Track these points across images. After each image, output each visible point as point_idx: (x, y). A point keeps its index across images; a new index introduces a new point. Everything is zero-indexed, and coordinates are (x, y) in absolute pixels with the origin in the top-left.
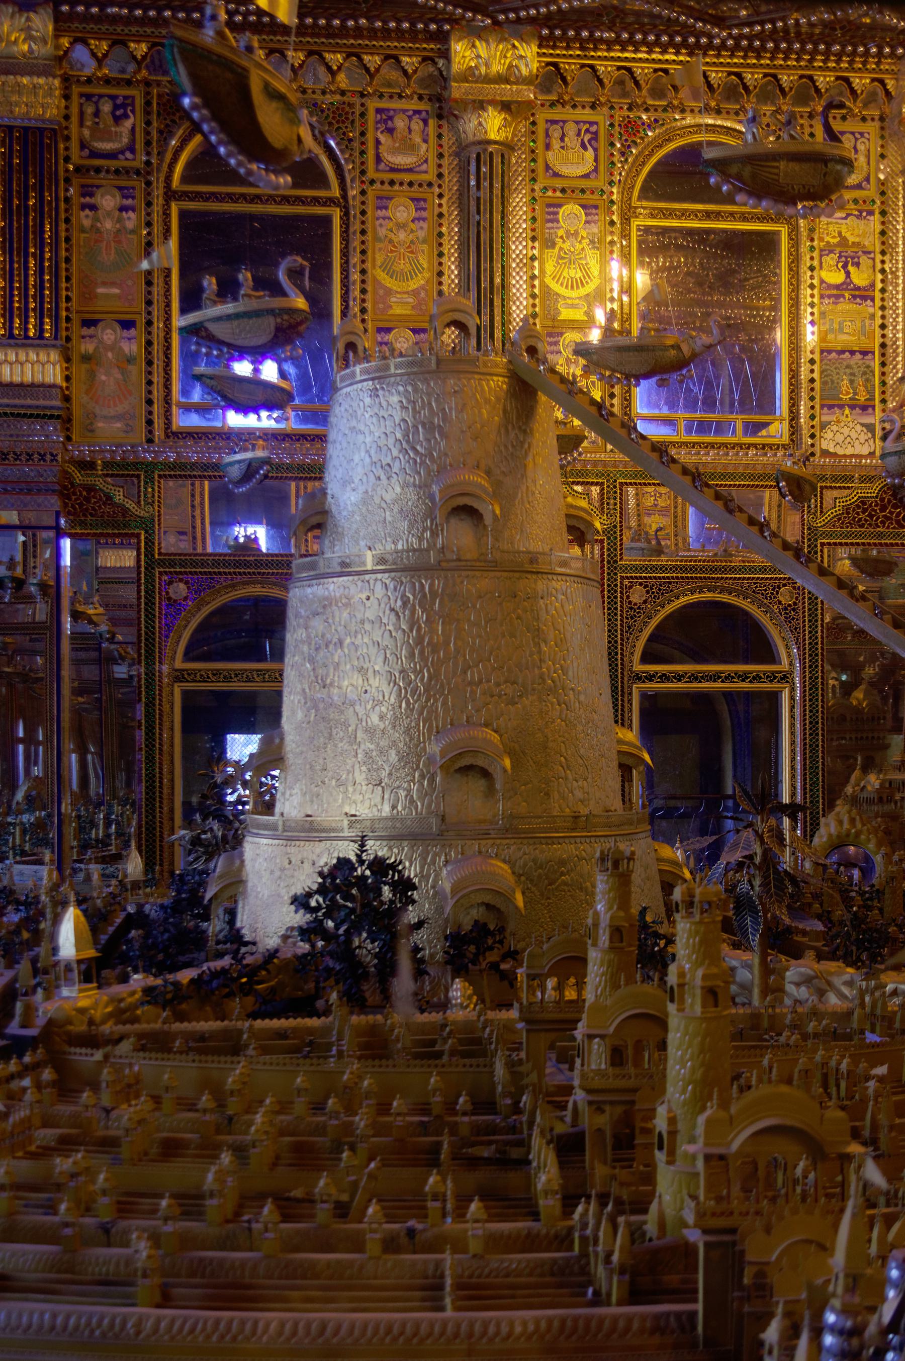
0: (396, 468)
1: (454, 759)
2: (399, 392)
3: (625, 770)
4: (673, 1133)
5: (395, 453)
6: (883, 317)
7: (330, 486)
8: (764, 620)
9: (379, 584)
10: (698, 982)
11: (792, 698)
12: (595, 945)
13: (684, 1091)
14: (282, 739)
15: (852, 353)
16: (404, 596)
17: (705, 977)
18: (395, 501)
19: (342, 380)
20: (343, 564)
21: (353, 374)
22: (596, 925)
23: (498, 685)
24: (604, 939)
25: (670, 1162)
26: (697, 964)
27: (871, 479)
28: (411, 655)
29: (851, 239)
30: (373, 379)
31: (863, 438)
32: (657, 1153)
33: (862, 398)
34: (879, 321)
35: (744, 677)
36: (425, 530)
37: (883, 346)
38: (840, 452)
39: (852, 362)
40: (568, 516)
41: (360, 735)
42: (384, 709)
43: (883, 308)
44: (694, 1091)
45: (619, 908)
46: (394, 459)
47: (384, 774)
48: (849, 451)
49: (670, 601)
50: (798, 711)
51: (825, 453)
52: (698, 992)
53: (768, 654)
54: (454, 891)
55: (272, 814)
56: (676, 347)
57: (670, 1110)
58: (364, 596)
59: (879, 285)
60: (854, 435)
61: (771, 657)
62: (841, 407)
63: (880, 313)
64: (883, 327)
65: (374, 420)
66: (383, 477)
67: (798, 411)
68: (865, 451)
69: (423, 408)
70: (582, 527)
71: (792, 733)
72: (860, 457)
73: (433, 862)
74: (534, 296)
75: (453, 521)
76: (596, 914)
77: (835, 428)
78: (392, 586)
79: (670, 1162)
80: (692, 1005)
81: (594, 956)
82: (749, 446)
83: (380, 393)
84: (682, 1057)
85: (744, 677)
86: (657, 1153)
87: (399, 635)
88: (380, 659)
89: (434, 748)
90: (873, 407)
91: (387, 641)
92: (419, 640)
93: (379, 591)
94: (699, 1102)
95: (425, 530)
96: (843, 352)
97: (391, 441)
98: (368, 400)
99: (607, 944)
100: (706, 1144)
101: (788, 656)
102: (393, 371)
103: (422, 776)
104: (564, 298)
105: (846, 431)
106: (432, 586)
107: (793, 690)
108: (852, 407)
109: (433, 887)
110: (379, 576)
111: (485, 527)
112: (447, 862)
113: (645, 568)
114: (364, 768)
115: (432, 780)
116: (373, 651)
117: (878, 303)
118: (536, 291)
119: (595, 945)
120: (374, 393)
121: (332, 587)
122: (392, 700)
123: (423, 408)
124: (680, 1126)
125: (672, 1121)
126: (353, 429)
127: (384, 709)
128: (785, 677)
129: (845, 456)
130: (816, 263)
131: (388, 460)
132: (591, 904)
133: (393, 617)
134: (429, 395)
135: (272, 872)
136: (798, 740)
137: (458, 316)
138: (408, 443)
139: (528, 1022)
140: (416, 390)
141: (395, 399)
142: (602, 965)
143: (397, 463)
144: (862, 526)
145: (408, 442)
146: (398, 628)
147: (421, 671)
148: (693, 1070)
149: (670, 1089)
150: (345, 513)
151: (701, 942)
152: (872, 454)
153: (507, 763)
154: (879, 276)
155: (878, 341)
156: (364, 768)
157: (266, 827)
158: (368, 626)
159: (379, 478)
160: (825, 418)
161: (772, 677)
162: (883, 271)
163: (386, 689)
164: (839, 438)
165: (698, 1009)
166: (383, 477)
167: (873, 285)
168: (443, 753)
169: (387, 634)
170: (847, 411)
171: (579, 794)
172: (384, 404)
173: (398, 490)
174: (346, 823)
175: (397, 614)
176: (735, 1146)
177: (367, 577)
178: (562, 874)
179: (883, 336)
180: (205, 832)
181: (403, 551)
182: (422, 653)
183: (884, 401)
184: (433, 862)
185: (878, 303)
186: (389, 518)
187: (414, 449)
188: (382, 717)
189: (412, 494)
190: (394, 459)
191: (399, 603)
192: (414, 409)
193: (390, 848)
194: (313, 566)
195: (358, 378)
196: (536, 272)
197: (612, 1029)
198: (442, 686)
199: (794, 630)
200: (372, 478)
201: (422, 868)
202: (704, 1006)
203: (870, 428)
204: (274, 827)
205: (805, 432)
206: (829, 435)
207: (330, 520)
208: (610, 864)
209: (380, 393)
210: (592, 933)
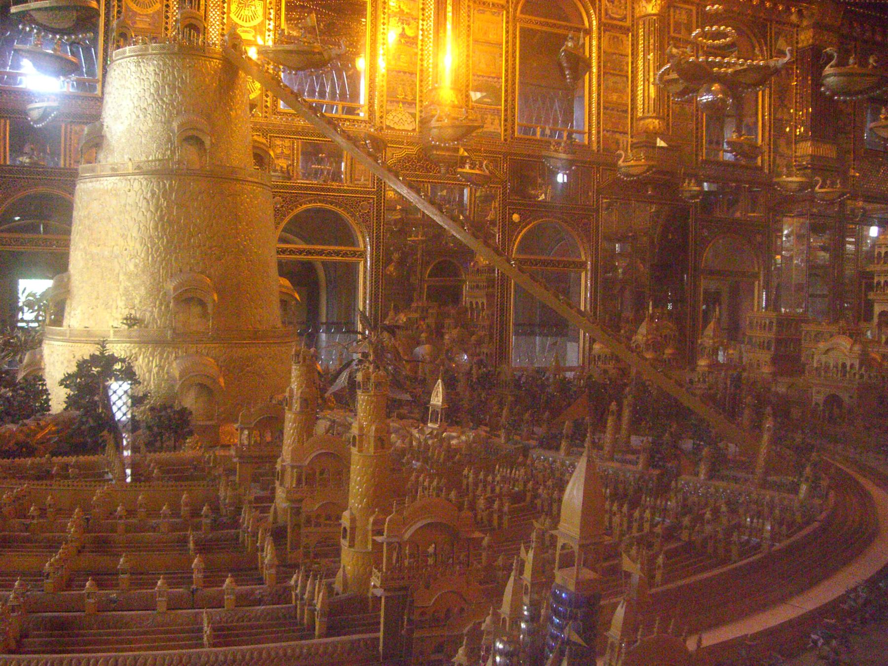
0: (150, 111)
1: (181, 294)
2: (154, 65)
3: (284, 303)
4: (353, 529)
5: (150, 101)
6: (422, 55)
7: (106, 120)
8: (351, 220)
9: (136, 181)
10: (372, 433)
11: (365, 267)
12: (290, 409)
13: (361, 502)
14: (69, 279)
15: (405, 73)
16: (152, 190)
17: (377, 430)
18: (148, 131)
19: (116, 55)
20: (113, 169)
21: (124, 53)
22: (291, 397)
23: (211, 248)
24: (296, 406)
25: (350, 546)
26: (372, 422)
27: (411, 144)
28: (156, 228)
29: (406, 11)
30: (137, 56)
31: (409, 120)
32: (342, 541)
33: (409, 98)
34: (419, 57)
35: (338, 253)
36: (167, 150)
37: (422, 71)
38: (397, 127)
39: (405, 78)
40: (254, 147)
41: (122, 277)
42: (137, 261)
43: (422, 50)
44: (368, 503)
45: (306, 387)
46: (149, 105)
47: (137, 302)
48: (401, 127)
49: (296, 207)
50: (368, 274)
51: (388, 127)
52: (372, 440)
53: (350, 240)
54: (181, 377)
55: (61, 326)
56: (320, 54)
57: (352, 514)
58: (127, 190)
59: (420, 38)
60: (404, 118)
61: (354, 243)
62: (398, 102)
63: (420, 53)
64: (422, 60)
65: (137, 80)
66: (141, 116)
67: (374, 103)
68: (410, 128)
69: (169, 75)
70: (262, 154)
71: (365, 288)
72: (408, 131)
73: (168, 357)
74: (223, 24)
75: (185, 145)
76: (291, 390)
77: (394, 114)
78: (145, 183)
79: (352, 545)
80: (368, 448)
81: (289, 416)
82: (346, 120)
83: (142, 64)
84: (360, 481)
85: (338, 253)
86: (342, 541)
87: (148, 215)
88: (136, 229)
89: (170, 286)
90: (415, 104)
91: (140, 218)
92: (161, 218)
93: (136, 185)
94: (369, 509)
95: (167, 150)
96: (400, 72)
97: (147, 94)
98: (133, 68)
99: (298, 409)
100: (388, 537)
101: (364, 243)
102: (150, 51)
103: (161, 304)
104: (241, 26)
105: (400, 116)
106: (170, 185)
107: (366, 262)
108: (404, 103)
109: (168, 373)
110: (137, 177)
111: (205, 150)
112: (176, 358)
113: (283, 187)
114: (124, 298)
115: (167, 306)
116: (131, 224)
117: (420, 47)
118: (225, 21)
119: (290, 409)
120: (138, 64)
121: (105, 183)
122: (143, 255)
123: (169, 75)
124: (358, 524)
125: (353, 520)
126: (123, 86)
127: (137, 261)
128: (362, 254)
129: (399, 130)
130: (386, 21)
131: (145, 106)
132: (288, 383)
133: (145, 203)
134: (173, 68)
135: (62, 363)
136: (368, 291)
137: (193, 21)
138: (158, 96)
139: (241, 458)
140: (165, 64)
141: (152, 68)
142: (294, 422)
143: (151, 108)
144: (407, 170)
145: (158, 95)
146: (148, 210)
147: (162, 237)
148: (367, 489)
149: (351, 501)
150: (115, 137)
151: (375, 407)
152: (414, 130)
153: (216, 297)
154: (421, 33)
155: (419, 68)
156: (124, 298)
157: (58, 334)
158: (128, 208)
159: (138, 117)
160: (389, 108)
161: (354, 254)
162: (422, 30)
163: (138, 246)
164: (396, 119)
165: (372, 450)
166: (141, 116)
167: (417, 37)
168: (175, 289)
169: (141, 213)
170: (401, 105)
171: (258, 317)
172: (144, 71)
173: (151, 125)
174: (112, 332)
175: (148, 202)
176: (407, 536)
177: (129, 177)
178: (248, 366)
179: (422, 65)
180: (13, 338)
181: (152, 161)
182: (163, 225)
183: (421, 101)
184: (168, 357)
185: (420, 47)
186: (143, 141)
187: (162, 100)
188: (136, 266)
189: (159, 127)
190: (149, 105)
191: (149, 194)
192: (163, 75)
193: (140, 349)
194: (93, 170)
195: (128, 54)
196: (225, 10)
197: (307, 462)
198: (175, 248)
199: (368, 227)
200: (134, 117)
201: (160, 361)
202: (375, 449)
203: (413, 115)
204: (63, 334)
205: (378, 114)
206: (391, 117)
207: (105, 142)
208: (301, 359)
209: (142, 64)
210: (288, 402)
